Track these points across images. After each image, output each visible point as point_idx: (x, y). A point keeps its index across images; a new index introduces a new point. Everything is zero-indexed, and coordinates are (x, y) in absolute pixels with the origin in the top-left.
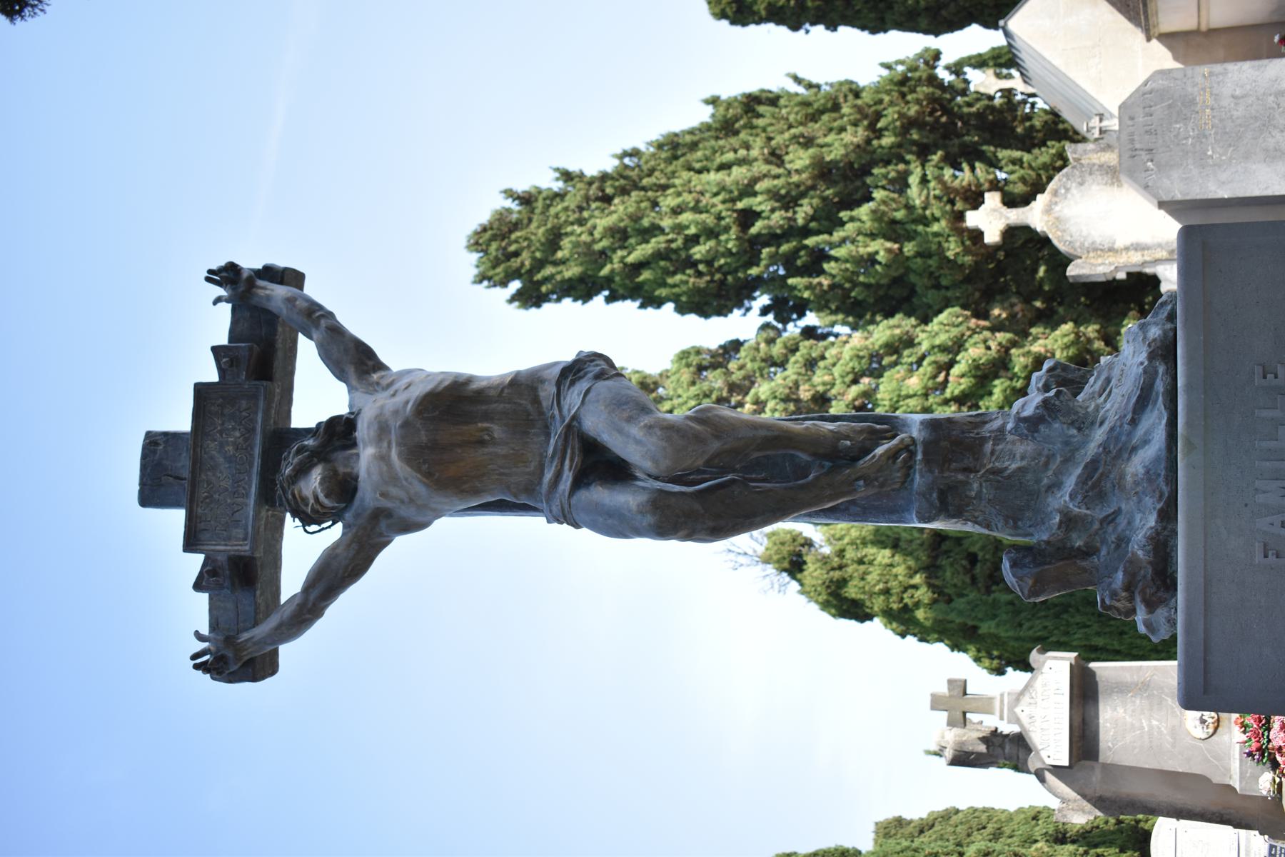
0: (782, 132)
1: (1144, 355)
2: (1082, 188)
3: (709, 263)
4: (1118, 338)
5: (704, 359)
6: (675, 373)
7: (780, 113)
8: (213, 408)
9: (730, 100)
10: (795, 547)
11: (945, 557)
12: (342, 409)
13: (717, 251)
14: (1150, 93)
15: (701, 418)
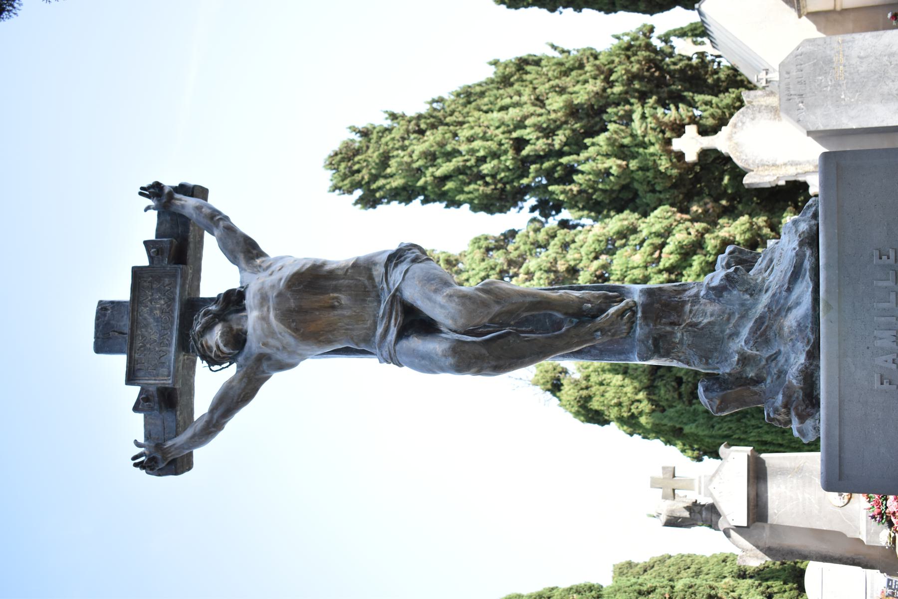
0: (544, 84)
1: (796, 243)
2: (754, 122)
3: (493, 176)
4: (780, 226)
5: (490, 243)
6: (470, 253)
7: (541, 71)
8: (145, 284)
9: (507, 62)
10: (555, 373)
11: (660, 380)
12: (236, 285)
13: (499, 168)
14: (801, 55)
15: (487, 290)
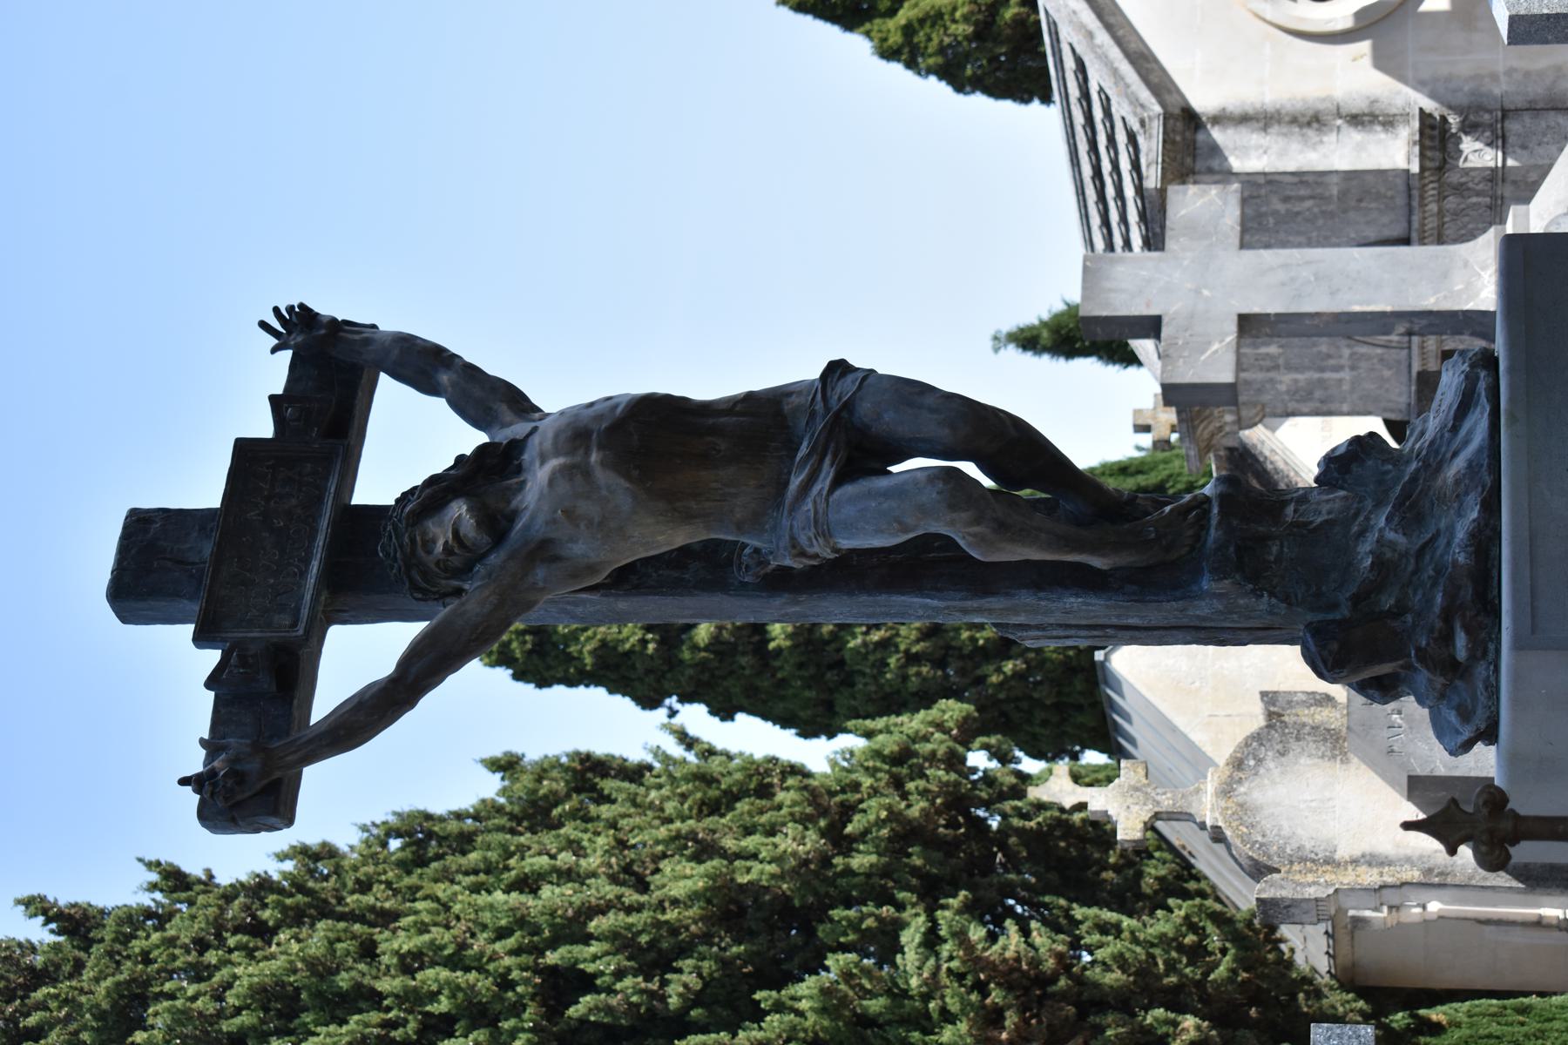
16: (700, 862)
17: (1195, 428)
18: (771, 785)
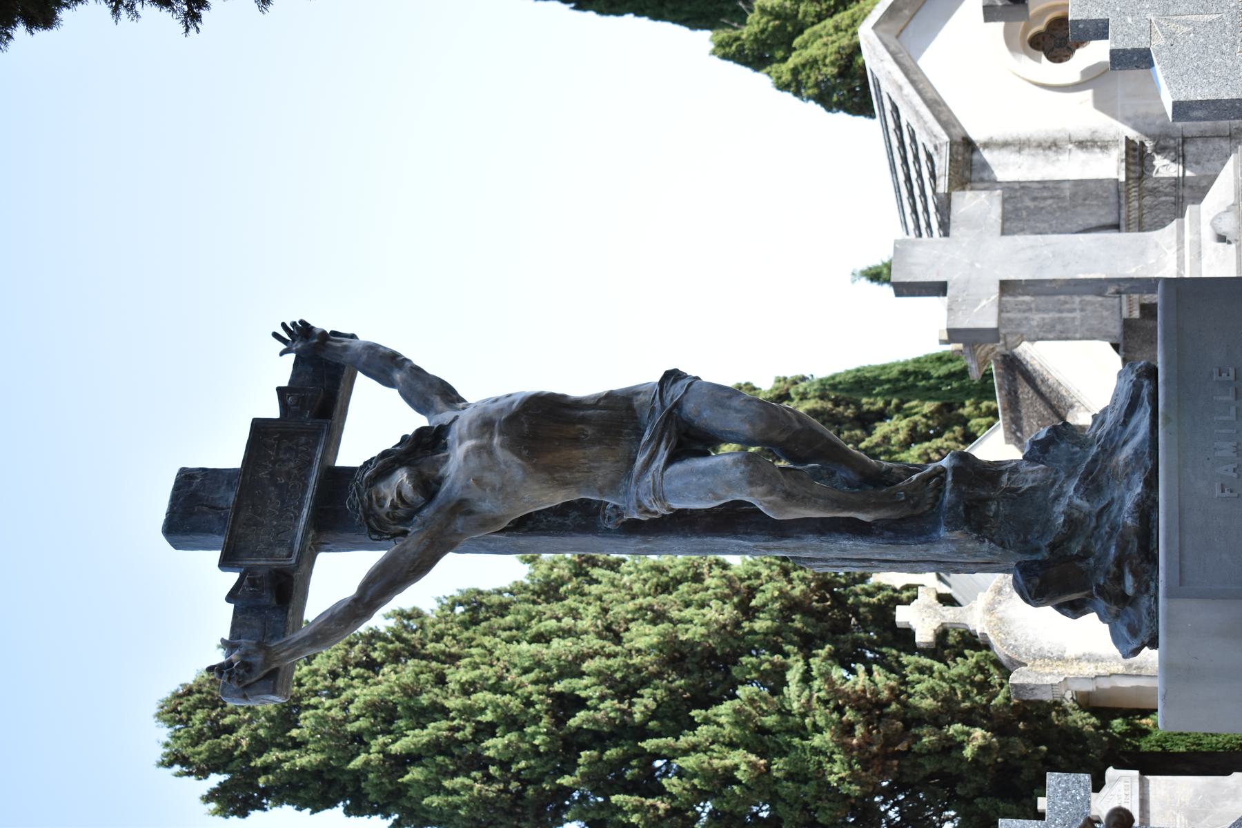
3: (505, 765)
13: (519, 748)
16: (655, 624)
17: (975, 350)
18: (702, 574)
